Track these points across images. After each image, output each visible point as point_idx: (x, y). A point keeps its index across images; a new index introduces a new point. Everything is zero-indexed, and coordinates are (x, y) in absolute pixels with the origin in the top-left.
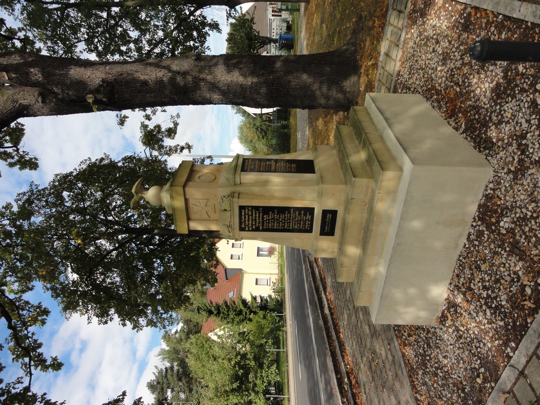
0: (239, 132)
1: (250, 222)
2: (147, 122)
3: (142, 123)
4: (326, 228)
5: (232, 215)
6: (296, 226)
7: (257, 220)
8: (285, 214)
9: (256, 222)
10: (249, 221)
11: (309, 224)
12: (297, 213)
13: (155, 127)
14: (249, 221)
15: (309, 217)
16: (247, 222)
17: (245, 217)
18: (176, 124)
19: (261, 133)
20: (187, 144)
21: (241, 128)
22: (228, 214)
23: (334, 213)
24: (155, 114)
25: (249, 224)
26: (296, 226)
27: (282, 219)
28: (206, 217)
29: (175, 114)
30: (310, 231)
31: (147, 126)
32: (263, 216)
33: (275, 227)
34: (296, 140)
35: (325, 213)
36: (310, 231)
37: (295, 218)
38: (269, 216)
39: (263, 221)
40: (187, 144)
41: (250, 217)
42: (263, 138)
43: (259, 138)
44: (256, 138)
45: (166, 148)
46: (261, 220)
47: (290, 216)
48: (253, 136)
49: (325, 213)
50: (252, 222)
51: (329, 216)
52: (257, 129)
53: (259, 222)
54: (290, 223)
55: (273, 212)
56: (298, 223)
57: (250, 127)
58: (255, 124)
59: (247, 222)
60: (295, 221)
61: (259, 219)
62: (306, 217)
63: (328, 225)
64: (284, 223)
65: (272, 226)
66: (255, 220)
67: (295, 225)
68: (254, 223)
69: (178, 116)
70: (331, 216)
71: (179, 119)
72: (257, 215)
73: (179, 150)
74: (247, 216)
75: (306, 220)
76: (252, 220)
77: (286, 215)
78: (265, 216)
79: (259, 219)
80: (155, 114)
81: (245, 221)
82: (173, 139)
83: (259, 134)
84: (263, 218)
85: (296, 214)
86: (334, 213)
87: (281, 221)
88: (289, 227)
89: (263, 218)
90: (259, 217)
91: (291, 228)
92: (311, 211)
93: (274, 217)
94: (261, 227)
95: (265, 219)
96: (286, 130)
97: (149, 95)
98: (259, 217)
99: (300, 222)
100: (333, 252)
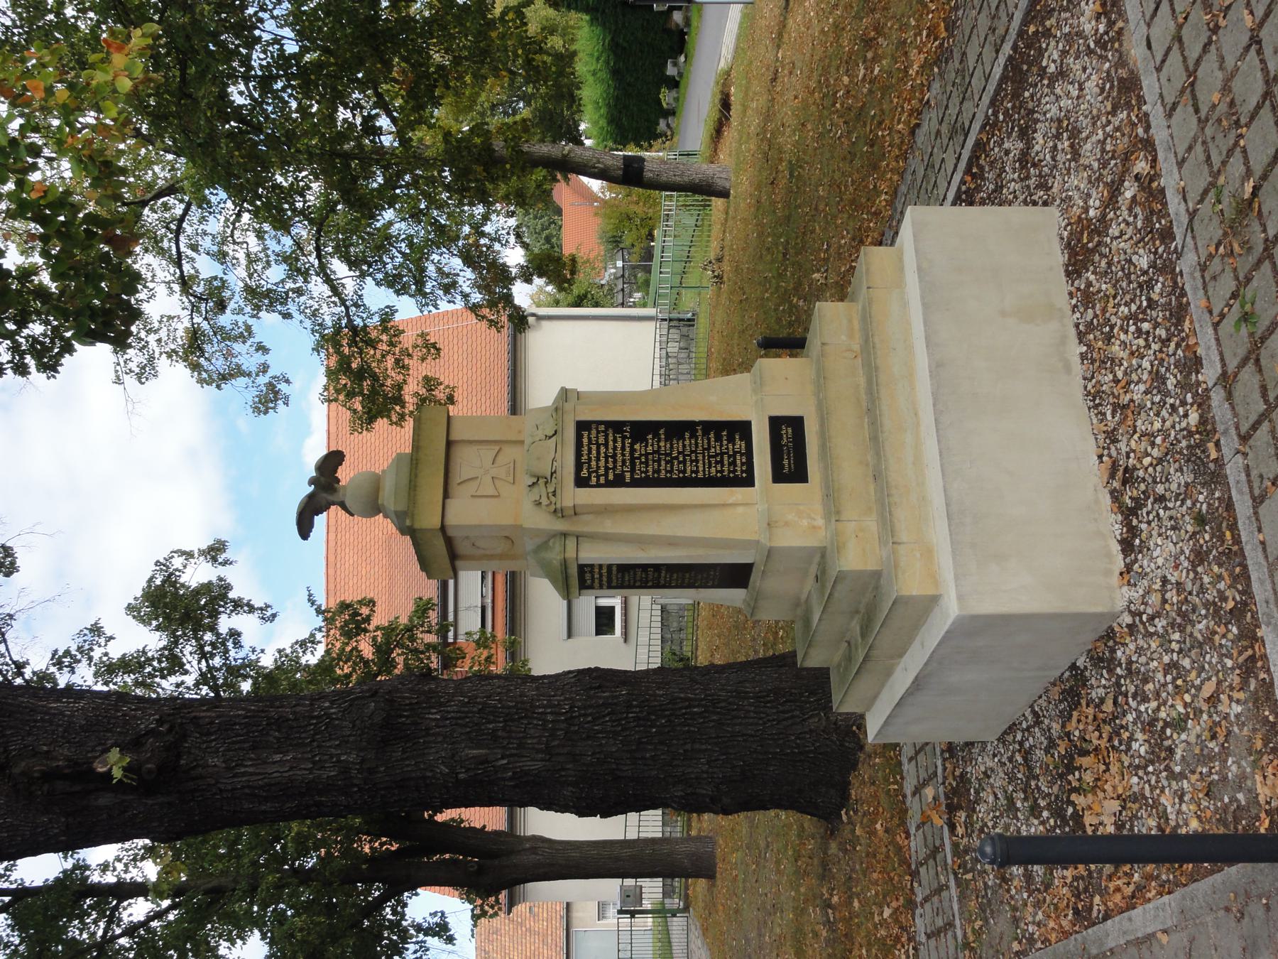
1: (602, 463)
4: (786, 462)
6: (713, 470)
7: (619, 458)
9: (615, 462)
10: (598, 459)
11: (743, 464)
12: (712, 435)
14: (598, 459)
23: (797, 423)
25: (598, 467)
26: (713, 470)
27: (679, 453)
33: (663, 474)
36: (748, 481)
37: (708, 449)
38: (646, 446)
39: (633, 459)
41: (603, 449)
50: (607, 462)
51: (787, 432)
53: (624, 462)
55: (656, 435)
56: (717, 462)
59: (593, 463)
60: (710, 457)
61: (623, 455)
64: (684, 462)
67: (710, 467)
68: (611, 465)
70: (790, 430)
72: (619, 445)
74: (594, 447)
75: (735, 453)
76: (606, 457)
77: (687, 442)
78: (637, 446)
79: (623, 455)
81: (590, 459)
84: (633, 450)
85: (709, 440)
86: (797, 423)
87: (677, 458)
88: (697, 472)
89: (633, 450)
90: (623, 448)
91: (700, 475)
92: (742, 429)
93: (659, 447)
94: (628, 475)
95: (637, 455)
97: (277, 757)
98: (623, 448)
100: (814, 527)
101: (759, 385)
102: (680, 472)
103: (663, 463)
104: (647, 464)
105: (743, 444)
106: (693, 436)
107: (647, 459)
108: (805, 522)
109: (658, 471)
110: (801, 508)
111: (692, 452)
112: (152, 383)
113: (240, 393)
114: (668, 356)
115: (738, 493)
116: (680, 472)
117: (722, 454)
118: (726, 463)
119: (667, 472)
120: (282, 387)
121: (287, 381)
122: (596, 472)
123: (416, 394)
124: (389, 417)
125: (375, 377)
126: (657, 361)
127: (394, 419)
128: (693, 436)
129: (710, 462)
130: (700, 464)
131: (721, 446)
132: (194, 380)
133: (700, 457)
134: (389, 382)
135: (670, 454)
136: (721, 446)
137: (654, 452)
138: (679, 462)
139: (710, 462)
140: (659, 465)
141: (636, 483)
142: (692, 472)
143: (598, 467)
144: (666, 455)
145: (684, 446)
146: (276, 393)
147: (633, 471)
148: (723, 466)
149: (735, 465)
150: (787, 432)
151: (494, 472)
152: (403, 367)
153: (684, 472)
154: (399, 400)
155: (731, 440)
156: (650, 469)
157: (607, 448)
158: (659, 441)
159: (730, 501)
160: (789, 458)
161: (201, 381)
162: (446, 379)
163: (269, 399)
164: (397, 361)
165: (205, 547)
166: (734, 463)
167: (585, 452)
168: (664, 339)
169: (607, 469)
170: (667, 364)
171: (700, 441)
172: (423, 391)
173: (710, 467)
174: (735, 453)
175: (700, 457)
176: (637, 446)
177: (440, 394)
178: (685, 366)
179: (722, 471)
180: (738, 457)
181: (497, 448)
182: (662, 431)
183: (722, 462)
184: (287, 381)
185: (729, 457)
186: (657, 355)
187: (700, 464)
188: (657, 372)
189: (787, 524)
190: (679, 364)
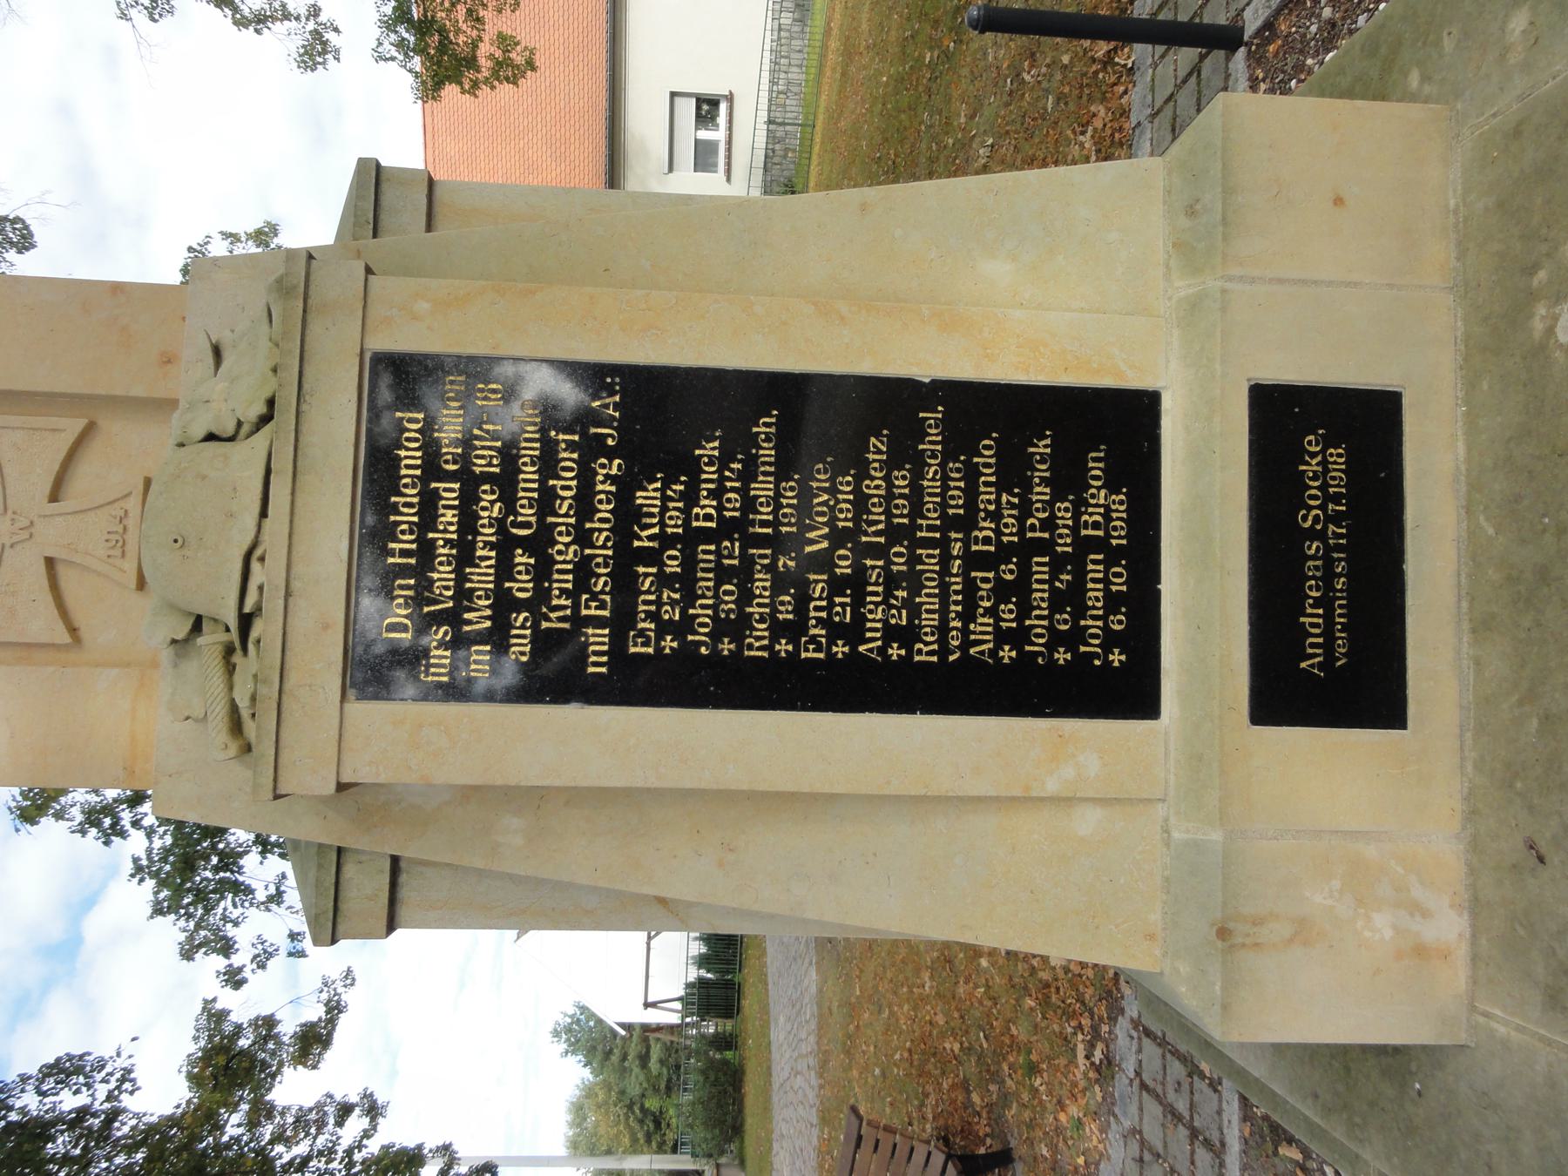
0: (572, 1125)
1: (482, 576)
2: (228, 999)
3: (208, 1004)
4: (1312, 618)
5: (282, 464)
6: (982, 626)
7: (565, 551)
8: (863, 474)
9: (542, 571)
10: (465, 557)
11: (1113, 602)
12: (987, 456)
13: (255, 1023)
14: (465, 557)
15: (1105, 503)
16: (443, 575)
17: (429, 504)
18: (335, 1009)
19: (641, 1122)
20: (368, 1096)
21: (578, 1110)
22: (248, 456)
23: (1366, 424)
24: (262, 966)
25: (463, 595)
26: (982, 626)
27: (838, 537)
28: (43, 624)
29: (335, 973)
30: (1128, 690)
31: (222, 1015)
32: (625, 487)
33: (757, 644)
34: (765, 1009)
35: (1284, 420)
36: (1128, 690)
37: (967, 523)
38: (690, 498)
39: (626, 559)
40: (368, 1096)
41: (489, 506)
42: (648, 1140)
43: (634, 1140)
44: (626, 1141)
45: (282, 1114)
46: (602, 549)
47: (916, 496)
48: (616, 1136)
49: (1284, 420)
50: (505, 569)
51: (1324, 464)
52: (630, 1107)
53: (583, 570)
54: (916, 588)
55: (739, 445)
56: (1002, 591)
57: (606, 1103)
58: (622, 1092)
59: (443, 575)
60: (973, 561)
61: (583, 538)
62: (1079, 506)
63: (1328, 577)
64: (856, 583)
65: (721, 628)
66: (540, 543)
67: (968, 616)
68: (521, 586)
69: (349, 977)
70: (1337, 457)
71: (352, 991)
72: (566, 485)
73: (331, 1121)
74: (449, 492)
75: (1084, 546)
76: (505, 545)
77: (874, 487)
78: (648, 497)
79: (583, 538)
80: (262, 966)
81: (426, 551)
82: (314, 1067)
83: (636, 1126)
84: (627, 516)
85: (971, 474)
86: (1366, 424)
87: (824, 562)
88: (907, 636)
89: (627, 516)
90: (585, 505)
91: (925, 653)
92: (1112, 431)
93: (749, 504)
94: (598, 639)
95: (644, 540)
96: (729, 1054)
98: (585, 505)
99: (1025, 572)
100: (1421, 951)
101: (1207, 228)
102: (835, 631)
103: (762, 583)
104: (686, 583)
105: (1119, 503)
106: (904, 454)
107: (690, 562)
108: (1383, 925)
109: (738, 627)
110: (1371, 851)
111: (894, 534)
112: (167, 21)
113: (283, 40)
114: (780, 30)
115: (1084, 746)
116: (835, 631)
117: (1026, 550)
118: (1040, 594)
119: (779, 630)
120: (330, 36)
121: (336, 30)
122: (453, 618)
123: (491, 57)
124: (460, 83)
125: (442, 31)
126: (768, 33)
127: (467, 87)
128: (904, 454)
129: (970, 588)
130: (928, 600)
131: (1025, 510)
132: (229, 20)
133: (930, 561)
134: (462, 39)
135: (800, 540)
136: (1025, 510)
137: (727, 528)
138: (836, 586)
139: (970, 588)
140: (746, 597)
141: (636, 683)
142: (891, 633)
143: (463, 595)
144: (777, 543)
145: (861, 503)
146: (325, 43)
147: (622, 623)
148: (1025, 610)
149: (1080, 611)
150: (1324, 464)
151: (54, 535)
152: (478, 19)
153: (854, 632)
154: (471, 62)
155: (1068, 482)
156: (701, 612)
157: (509, 501)
158: (748, 475)
159: (1052, 787)
160: (1325, 602)
161: (236, 23)
162: (525, 37)
163: (316, 51)
164: (470, 12)
165: (250, 230)
166: (1070, 599)
167: (409, 516)
168: (777, 7)
169: (504, 605)
170: (779, 38)
171: (930, 484)
172: (498, 54)
173: (968, 616)
174: (1084, 546)
175: (930, 561)
176: (648, 497)
177: (518, 58)
178: (798, 42)
179: (1019, 637)
180: (1095, 570)
181: (76, 426)
182: (764, 427)
183: (1020, 590)
184: (336, 30)
185: (1057, 565)
186: (769, 27)
187: (928, 600)
188: (767, 47)
189: (1303, 932)
190: (792, 38)
